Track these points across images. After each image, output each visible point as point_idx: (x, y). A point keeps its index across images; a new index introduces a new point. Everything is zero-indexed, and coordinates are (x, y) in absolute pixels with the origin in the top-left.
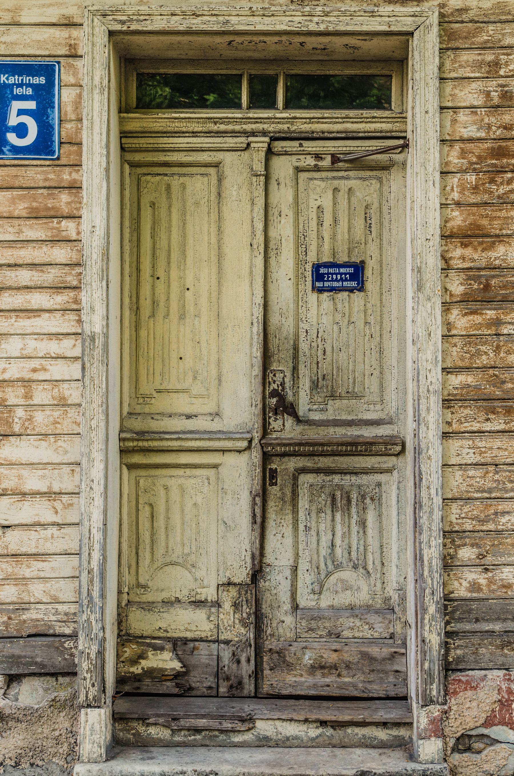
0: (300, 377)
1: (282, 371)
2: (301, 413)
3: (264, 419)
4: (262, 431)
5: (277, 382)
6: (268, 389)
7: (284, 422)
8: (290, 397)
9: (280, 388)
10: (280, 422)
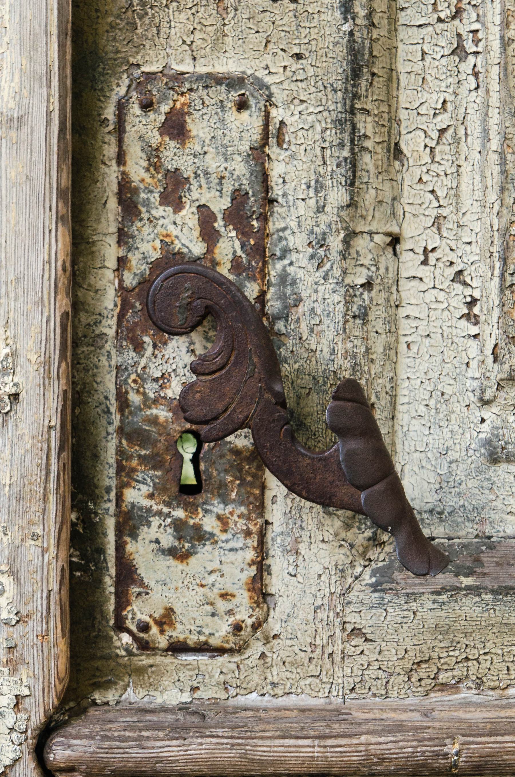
0: (412, 144)
1: (242, 91)
2: (417, 486)
3: (82, 540)
4: (59, 648)
5: (200, 194)
6: (110, 252)
7: (262, 566)
8: (319, 335)
9: (229, 246)
10: (226, 562)
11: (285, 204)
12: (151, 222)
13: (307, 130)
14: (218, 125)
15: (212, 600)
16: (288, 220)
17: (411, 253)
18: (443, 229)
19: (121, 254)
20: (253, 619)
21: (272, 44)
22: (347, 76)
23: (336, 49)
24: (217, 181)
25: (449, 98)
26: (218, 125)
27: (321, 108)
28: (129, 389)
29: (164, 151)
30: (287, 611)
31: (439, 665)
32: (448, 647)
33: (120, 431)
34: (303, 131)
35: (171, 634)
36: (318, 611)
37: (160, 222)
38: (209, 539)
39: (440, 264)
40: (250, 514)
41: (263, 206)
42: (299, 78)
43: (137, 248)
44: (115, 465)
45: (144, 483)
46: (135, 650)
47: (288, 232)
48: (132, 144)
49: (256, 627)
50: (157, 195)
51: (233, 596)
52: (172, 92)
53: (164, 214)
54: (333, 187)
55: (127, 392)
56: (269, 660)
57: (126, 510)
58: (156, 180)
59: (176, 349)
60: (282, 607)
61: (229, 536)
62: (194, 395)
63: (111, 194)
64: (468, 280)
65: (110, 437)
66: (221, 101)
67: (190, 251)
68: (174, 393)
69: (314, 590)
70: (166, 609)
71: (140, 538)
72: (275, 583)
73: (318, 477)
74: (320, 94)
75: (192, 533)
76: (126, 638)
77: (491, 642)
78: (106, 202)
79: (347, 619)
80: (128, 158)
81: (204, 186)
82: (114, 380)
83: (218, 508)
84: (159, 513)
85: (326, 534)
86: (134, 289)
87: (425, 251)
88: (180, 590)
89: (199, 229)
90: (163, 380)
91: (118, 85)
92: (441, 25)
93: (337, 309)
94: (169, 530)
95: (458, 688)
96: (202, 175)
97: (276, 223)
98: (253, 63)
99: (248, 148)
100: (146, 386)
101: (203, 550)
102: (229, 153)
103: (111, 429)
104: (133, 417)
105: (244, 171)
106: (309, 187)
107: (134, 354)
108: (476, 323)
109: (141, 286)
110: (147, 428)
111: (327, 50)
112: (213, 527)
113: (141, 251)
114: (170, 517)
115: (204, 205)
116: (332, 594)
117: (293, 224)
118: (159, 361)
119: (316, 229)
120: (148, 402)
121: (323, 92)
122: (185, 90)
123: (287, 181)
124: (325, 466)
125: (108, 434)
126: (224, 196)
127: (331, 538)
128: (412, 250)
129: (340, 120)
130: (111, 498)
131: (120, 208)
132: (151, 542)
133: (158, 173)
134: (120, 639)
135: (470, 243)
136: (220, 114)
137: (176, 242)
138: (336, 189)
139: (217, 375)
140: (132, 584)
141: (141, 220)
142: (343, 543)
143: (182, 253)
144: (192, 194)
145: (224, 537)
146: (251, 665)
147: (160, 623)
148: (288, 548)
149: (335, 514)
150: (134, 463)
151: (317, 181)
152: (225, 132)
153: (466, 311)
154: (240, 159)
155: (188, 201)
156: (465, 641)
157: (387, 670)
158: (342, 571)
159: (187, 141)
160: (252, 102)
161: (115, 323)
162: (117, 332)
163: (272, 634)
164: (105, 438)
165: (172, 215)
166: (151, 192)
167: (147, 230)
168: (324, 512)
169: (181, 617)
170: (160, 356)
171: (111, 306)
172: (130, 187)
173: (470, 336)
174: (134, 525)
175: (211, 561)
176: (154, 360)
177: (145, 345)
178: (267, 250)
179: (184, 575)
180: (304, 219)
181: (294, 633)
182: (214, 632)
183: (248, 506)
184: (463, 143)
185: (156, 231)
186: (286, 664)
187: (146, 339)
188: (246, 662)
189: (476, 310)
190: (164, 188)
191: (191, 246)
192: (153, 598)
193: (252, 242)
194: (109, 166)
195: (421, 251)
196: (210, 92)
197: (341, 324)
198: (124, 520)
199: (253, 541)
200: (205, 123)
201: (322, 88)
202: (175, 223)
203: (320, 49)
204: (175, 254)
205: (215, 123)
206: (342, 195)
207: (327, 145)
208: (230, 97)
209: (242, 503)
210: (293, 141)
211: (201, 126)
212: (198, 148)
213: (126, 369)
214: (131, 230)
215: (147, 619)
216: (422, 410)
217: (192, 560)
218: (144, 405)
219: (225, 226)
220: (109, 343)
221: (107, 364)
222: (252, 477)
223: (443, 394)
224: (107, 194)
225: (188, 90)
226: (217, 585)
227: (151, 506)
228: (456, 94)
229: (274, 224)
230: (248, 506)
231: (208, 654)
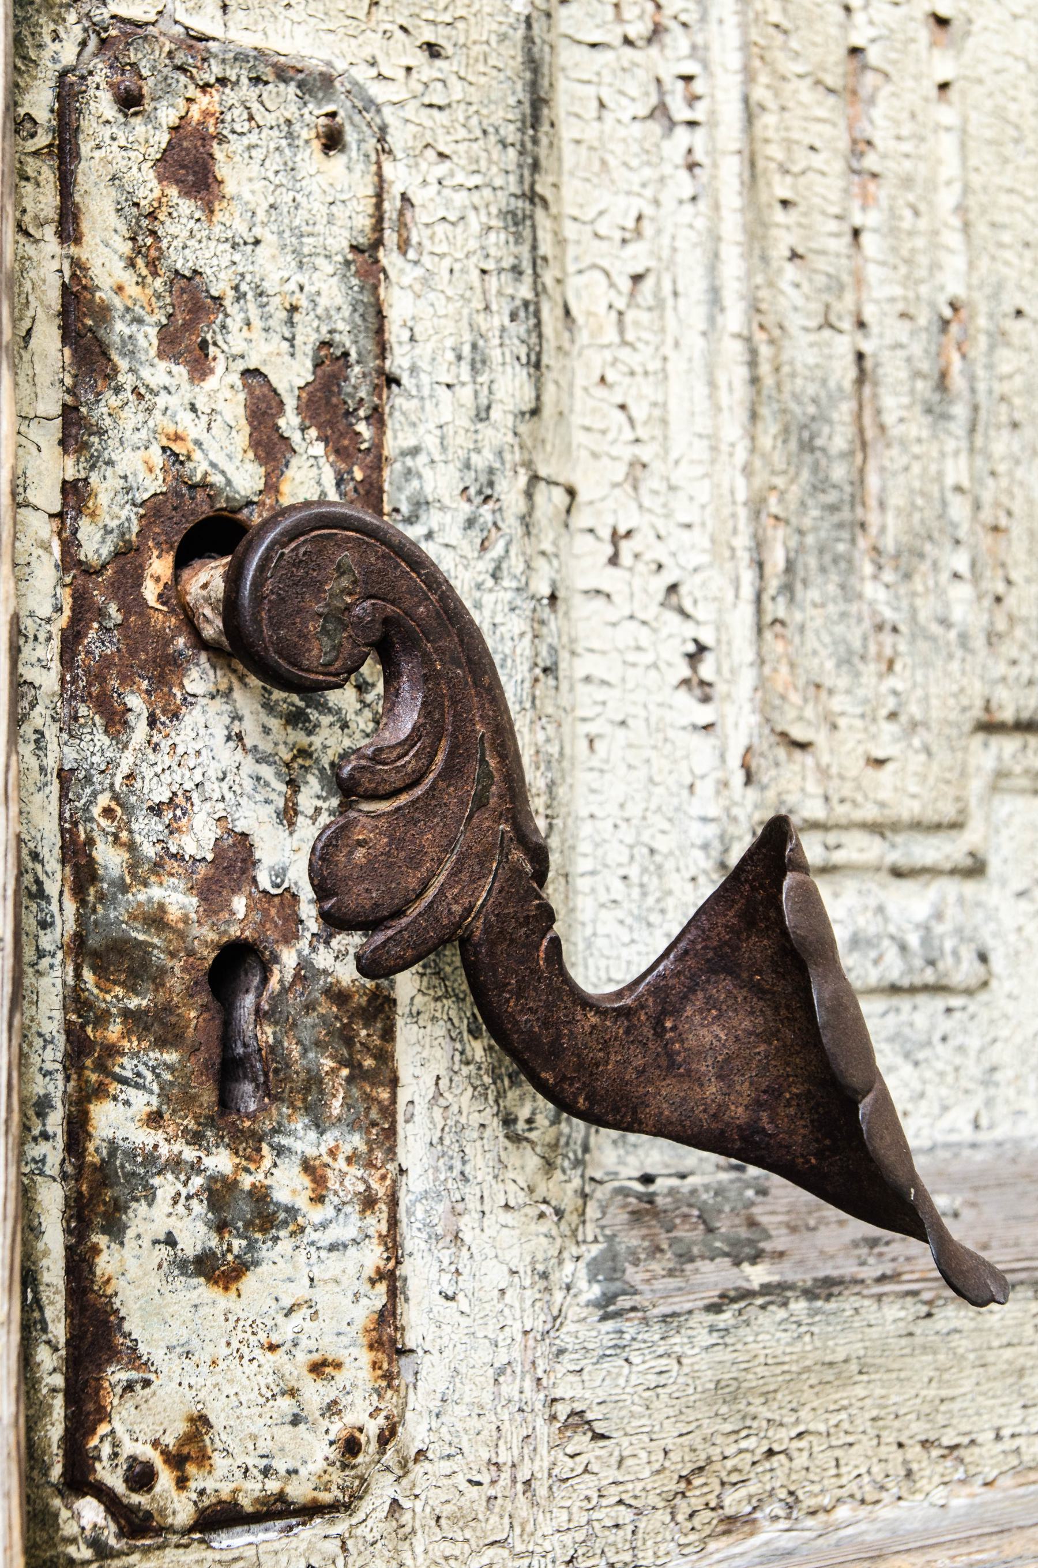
5: (243, 339)
11: (414, 392)
12: (140, 397)
13: (453, 224)
14: (281, 178)
15: (293, 1383)
16: (421, 429)
17: (589, 537)
18: (643, 490)
19: (70, 475)
20: (381, 1421)
21: (382, 10)
22: (524, 115)
23: (502, 49)
24: (284, 315)
25: (648, 211)
26: (281, 178)
27: (477, 180)
28: (95, 834)
29: (168, 221)
30: (441, 1388)
31: (723, 1474)
32: (737, 1432)
33: (79, 947)
34: (446, 225)
35: (201, 1485)
36: (501, 1379)
37: (162, 400)
38: (285, 1223)
39: (641, 567)
40: (371, 1151)
41: (376, 389)
42: (436, 101)
43: (110, 463)
44: (61, 1039)
45: (137, 1086)
46: (112, 1541)
47: (422, 459)
48: (94, 190)
49: (386, 1437)
50: (153, 332)
51: (338, 1366)
52: (183, 79)
53: (167, 381)
54: (504, 364)
55: (90, 842)
56: (406, 1518)
57: (97, 1160)
58: (149, 291)
59: (202, 731)
60: (429, 1377)
61: (326, 1211)
62: (351, 853)
63: (41, 315)
64: (688, 605)
65: (45, 962)
66: (289, 122)
67: (229, 482)
68: (200, 847)
69: (493, 1325)
70: (192, 1420)
71: (130, 1234)
72: (417, 1322)
73: (613, 1057)
74: (475, 146)
75: (246, 1208)
76: (90, 1512)
77: (808, 1407)
78: (29, 332)
79: (558, 1393)
80: (85, 226)
81: (257, 324)
82: (54, 807)
83: (304, 1140)
84: (176, 1164)
85: (512, 1188)
86: (104, 567)
87: (615, 538)
88: (222, 1365)
89: (247, 430)
90: (172, 809)
91: (56, 37)
92: (628, 51)
93: (518, 651)
94: (199, 1208)
95: (754, 1521)
96: (250, 296)
97: (400, 434)
98: (344, 46)
99: (345, 244)
100: (135, 826)
101: (273, 1255)
102: (306, 250)
103: (48, 941)
104: (106, 908)
105: (339, 300)
106: (459, 358)
107: (106, 741)
108: (706, 699)
109: (122, 560)
110: (141, 937)
111: (485, 47)
112: (294, 1191)
113: (120, 469)
114: (199, 1172)
115: (256, 372)
116: (526, 1333)
117: (431, 442)
118: (164, 759)
119: (475, 458)
120: (142, 868)
121: (481, 142)
122: (212, 80)
123: (417, 337)
124: (627, 1032)
125: (41, 954)
126: (299, 354)
127: (522, 1197)
128: (591, 531)
129: (514, 214)
130: (50, 1130)
131: (67, 351)
132: (156, 1242)
133: (155, 274)
134: (76, 1516)
135: (689, 526)
136: (287, 151)
137: (197, 455)
138: (509, 369)
139: (404, 799)
140: (109, 1362)
141: (118, 390)
142: (543, 1207)
143: (212, 486)
144: (229, 338)
145: (316, 1214)
146: (370, 1538)
147: (177, 1461)
148: (439, 1230)
149: (527, 1139)
150: (114, 1031)
151: (474, 346)
152: (298, 197)
153: (685, 672)
154: (330, 270)
155: (221, 357)
156: (765, 1412)
157: (632, 1502)
158: (545, 1276)
159: (217, 207)
160: (350, 136)
161: (57, 657)
162: (62, 680)
163: (413, 1454)
164: (33, 965)
165: (186, 386)
166: (139, 321)
167: (131, 417)
168: (507, 1137)
169: (224, 1437)
170: (165, 746)
171: (45, 610)
172: (92, 301)
173: (695, 727)
174: (116, 1200)
175: (290, 1280)
176: (152, 757)
177: (131, 717)
178: (385, 497)
179: (231, 1324)
180: (451, 433)
181: (456, 1440)
182: (297, 1465)
183: (368, 1132)
184: (669, 313)
185: (151, 424)
186: (443, 1521)
187: (135, 702)
188: (359, 1531)
189: (707, 670)
190: (170, 316)
191: (230, 469)
192: (161, 1392)
193: (359, 475)
194: (37, 241)
195: (606, 534)
196: (265, 96)
197: (527, 685)
198: (90, 1188)
199: (377, 1223)
200: (255, 166)
201: (478, 133)
202: (193, 408)
203: (475, 43)
204: (193, 487)
205: (277, 172)
206: (521, 387)
207: (490, 265)
208: (307, 116)
209: (353, 1126)
210: (426, 243)
211: (246, 173)
212: (240, 227)
213: (88, 780)
214: (96, 414)
215: (148, 1453)
216: (618, 889)
217: (249, 1282)
218: (134, 875)
219: (303, 429)
220: (39, 709)
221: (34, 763)
222: (375, 1057)
223: (652, 851)
224: (30, 313)
225: (218, 80)
226: (305, 1343)
227: (156, 1146)
228: (657, 202)
229: (395, 438)
230: (368, 1132)
231: (280, 1524)
